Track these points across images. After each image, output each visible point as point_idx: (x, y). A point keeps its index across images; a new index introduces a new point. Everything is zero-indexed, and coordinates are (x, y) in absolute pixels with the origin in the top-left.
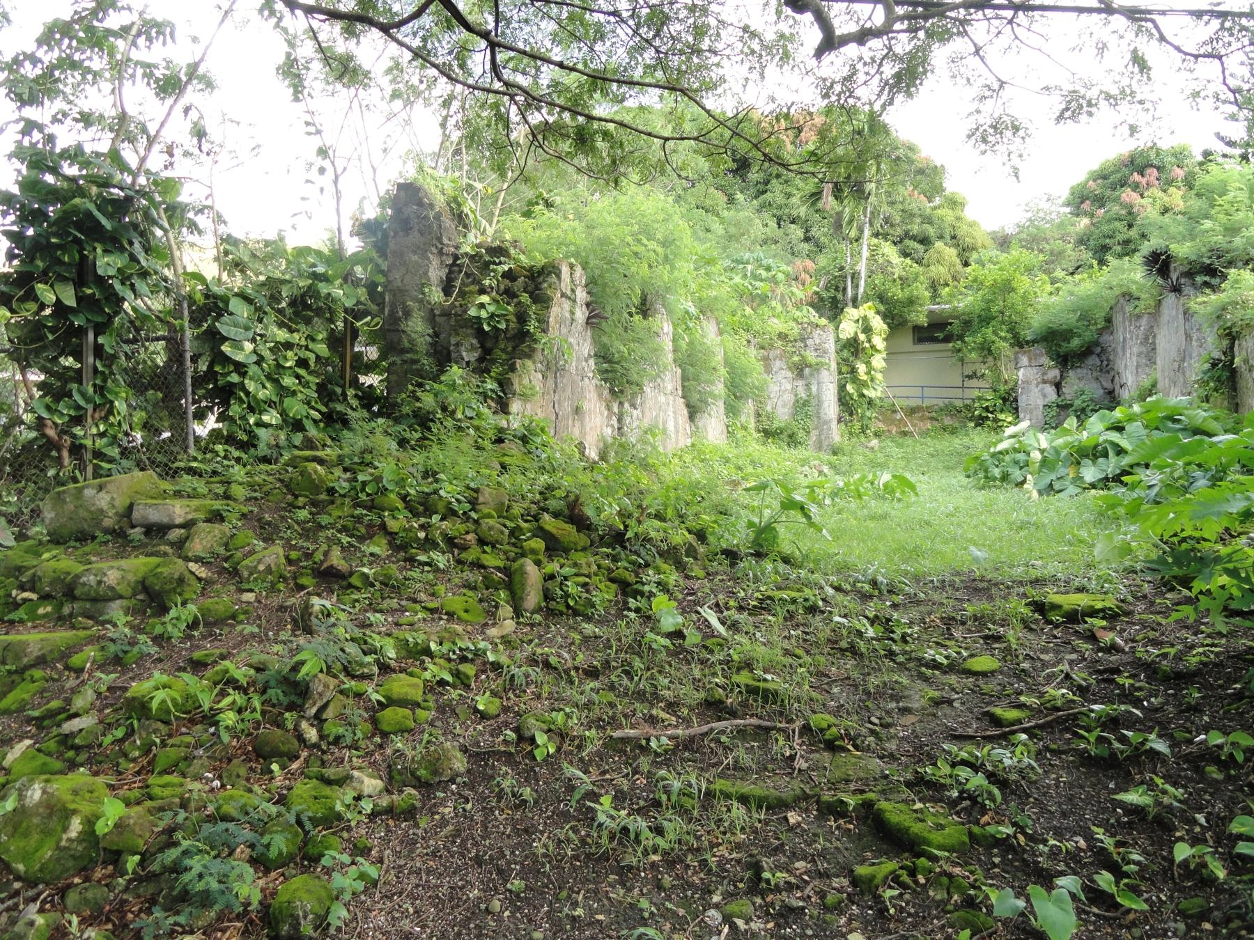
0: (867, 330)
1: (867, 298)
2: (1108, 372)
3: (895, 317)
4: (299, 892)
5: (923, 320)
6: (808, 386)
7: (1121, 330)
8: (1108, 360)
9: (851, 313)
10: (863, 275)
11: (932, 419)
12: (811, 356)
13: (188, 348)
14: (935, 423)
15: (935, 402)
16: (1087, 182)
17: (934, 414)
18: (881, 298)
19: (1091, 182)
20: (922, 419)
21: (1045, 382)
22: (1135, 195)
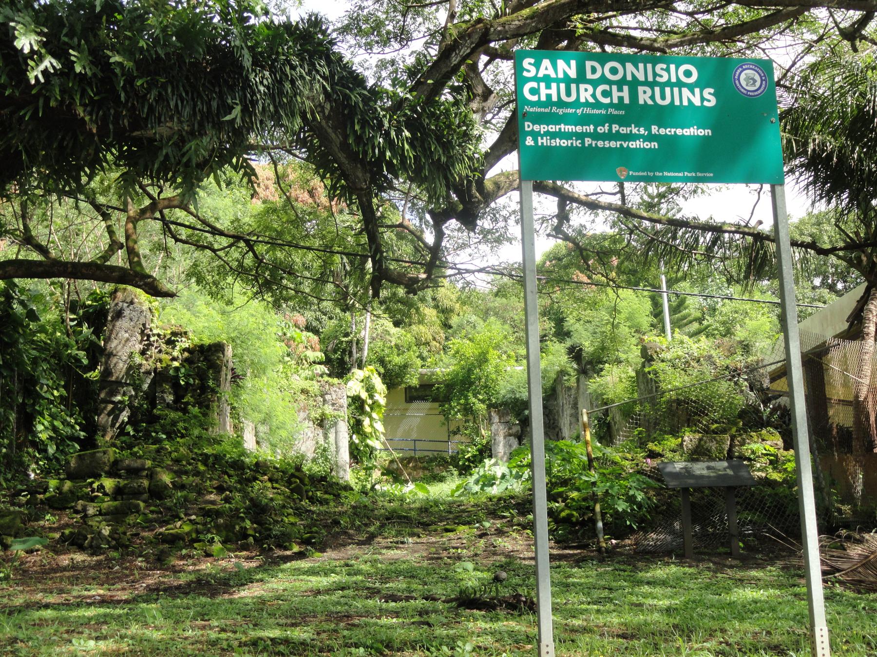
0: (370, 389)
1: (370, 363)
2: (554, 428)
3: (392, 378)
4: (48, 495)
5: (414, 382)
6: (326, 437)
7: (561, 397)
8: (554, 419)
9: (358, 374)
10: (367, 341)
11: (424, 468)
12: (328, 410)
13: (523, 629)
14: (426, 472)
15: (426, 453)
16: (545, 263)
17: (425, 464)
18: (382, 361)
19: (548, 263)
20: (415, 468)
21: (510, 435)
22: (229, 411)
